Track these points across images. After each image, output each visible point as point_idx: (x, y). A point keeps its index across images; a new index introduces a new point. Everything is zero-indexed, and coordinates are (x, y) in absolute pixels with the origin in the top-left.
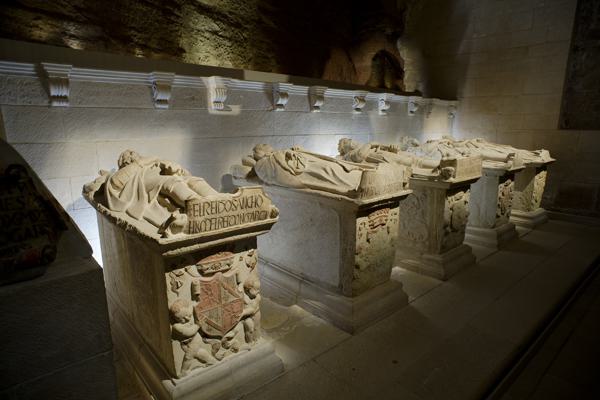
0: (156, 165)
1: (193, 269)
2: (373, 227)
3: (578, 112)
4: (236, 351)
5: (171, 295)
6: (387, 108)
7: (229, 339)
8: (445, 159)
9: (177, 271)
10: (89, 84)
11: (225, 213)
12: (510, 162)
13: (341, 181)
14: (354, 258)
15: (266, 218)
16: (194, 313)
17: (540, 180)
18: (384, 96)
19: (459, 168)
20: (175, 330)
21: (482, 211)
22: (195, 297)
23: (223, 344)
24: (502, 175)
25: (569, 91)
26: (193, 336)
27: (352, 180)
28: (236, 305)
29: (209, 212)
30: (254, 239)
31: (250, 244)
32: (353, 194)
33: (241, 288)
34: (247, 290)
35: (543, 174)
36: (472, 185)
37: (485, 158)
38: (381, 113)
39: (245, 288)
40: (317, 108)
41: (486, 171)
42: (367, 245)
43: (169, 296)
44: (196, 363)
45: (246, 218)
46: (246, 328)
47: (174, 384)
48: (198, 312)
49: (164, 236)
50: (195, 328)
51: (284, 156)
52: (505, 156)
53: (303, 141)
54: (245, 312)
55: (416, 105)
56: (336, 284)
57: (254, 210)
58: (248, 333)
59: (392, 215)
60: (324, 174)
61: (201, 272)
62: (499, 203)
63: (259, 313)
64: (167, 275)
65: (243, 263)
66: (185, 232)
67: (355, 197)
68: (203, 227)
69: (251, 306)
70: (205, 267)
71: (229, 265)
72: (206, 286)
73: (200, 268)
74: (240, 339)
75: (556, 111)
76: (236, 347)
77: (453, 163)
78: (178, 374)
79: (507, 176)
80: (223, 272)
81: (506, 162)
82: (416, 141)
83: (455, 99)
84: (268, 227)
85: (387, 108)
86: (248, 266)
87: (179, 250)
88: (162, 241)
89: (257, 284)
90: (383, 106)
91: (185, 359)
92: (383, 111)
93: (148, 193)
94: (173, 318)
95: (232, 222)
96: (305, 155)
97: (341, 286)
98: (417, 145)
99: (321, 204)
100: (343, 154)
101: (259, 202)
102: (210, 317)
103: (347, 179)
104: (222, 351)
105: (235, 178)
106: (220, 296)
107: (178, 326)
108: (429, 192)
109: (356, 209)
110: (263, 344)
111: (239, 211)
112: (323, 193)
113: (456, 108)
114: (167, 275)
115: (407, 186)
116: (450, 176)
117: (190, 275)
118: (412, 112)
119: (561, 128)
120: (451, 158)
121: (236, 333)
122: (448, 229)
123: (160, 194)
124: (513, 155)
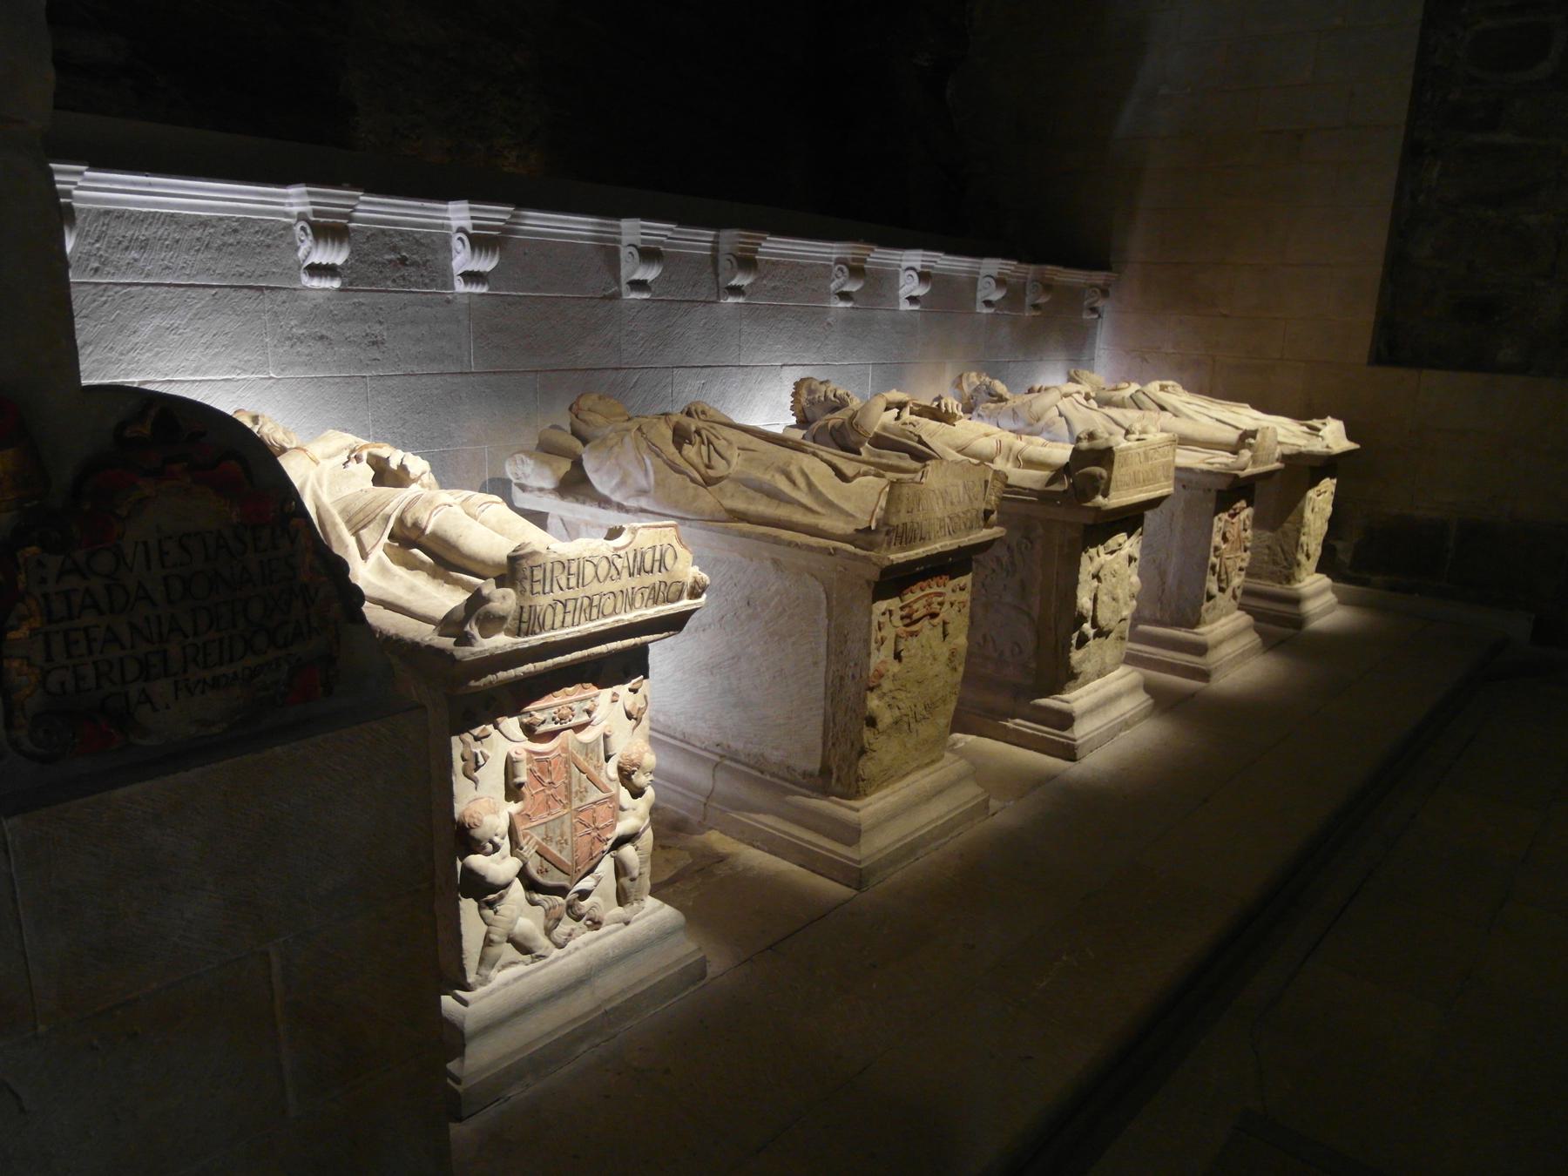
0: (358, 459)
1: (511, 724)
2: (909, 619)
3: (1425, 322)
4: (596, 924)
5: (460, 784)
6: (921, 291)
7: (584, 895)
8: (1084, 445)
9: (477, 731)
10: (120, 215)
11: (594, 588)
12: (1246, 454)
13: (830, 504)
14: (864, 701)
15: (679, 598)
16: (512, 832)
17: (1320, 500)
18: (914, 258)
19: (1119, 472)
20: (469, 872)
21: (1171, 580)
22: (513, 791)
23: (570, 907)
24: (1223, 486)
25: (1397, 263)
26: (507, 885)
27: (862, 497)
28: (602, 811)
29: (563, 583)
30: (643, 650)
31: (630, 666)
32: (864, 537)
33: (611, 769)
34: (625, 776)
35: (1328, 485)
36: (1149, 514)
37: (1184, 441)
38: (905, 306)
39: (620, 770)
40: (736, 291)
41: (1184, 476)
42: (895, 667)
43: (456, 789)
44: (509, 952)
45: (638, 598)
46: (621, 869)
47: (465, 1003)
48: (521, 827)
49: (464, 640)
50: (513, 865)
51: (669, 434)
52: (1232, 436)
53: (698, 383)
54: (623, 827)
55: (1000, 282)
56: (814, 765)
57: (657, 577)
58: (625, 881)
59: (954, 594)
60: (783, 484)
61: (529, 730)
62: (1213, 559)
63: (649, 832)
64: (455, 740)
65: (619, 709)
66: (509, 632)
67: (870, 546)
68: (548, 623)
69: (634, 816)
70: (539, 716)
71: (589, 712)
72: (540, 760)
73: (526, 720)
74: (605, 897)
75: (1363, 320)
76: (597, 914)
77: (1105, 456)
78: (471, 978)
79: (1231, 491)
80: (579, 728)
81: (1235, 452)
82: (1000, 387)
83: (1102, 265)
84: (675, 623)
85: (921, 291)
86: (629, 716)
87: (491, 677)
88: (463, 653)
89: (650, 759)
90: (910, 286)
91: (488, 942)
92: (913, 300)
93: (356, 534)
94: (467, 840)
95: (608, 605)
96: (727, 432)
97: (825, 771)
98: (1001, 399)
99: (775, 562)
100: (803, 422)
101: (669, 560)
102: (547, 839)
103: (848, 499)
104: (566, 925)
105: (523, 488)
106: (568, 787)
107: (476, 861)
108: (1040, 531)
109: (873, 574)
110: (653, 912)
111: (626, 582)
112: (787, 535)
113: (1105, 293)
114: (455, 740)
115: (994, 517)
116: (1096, 491)
117: (503, 741)
118: (988, 303)
119: (1377, 359)
120: (1099, 444)
121: (599, 880)
122: (1087, 626)
123: (391, 537)
124: (1253, 434)
